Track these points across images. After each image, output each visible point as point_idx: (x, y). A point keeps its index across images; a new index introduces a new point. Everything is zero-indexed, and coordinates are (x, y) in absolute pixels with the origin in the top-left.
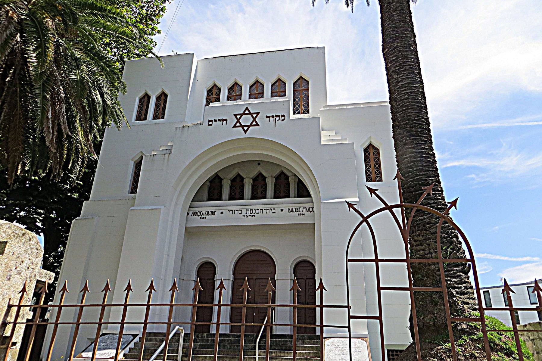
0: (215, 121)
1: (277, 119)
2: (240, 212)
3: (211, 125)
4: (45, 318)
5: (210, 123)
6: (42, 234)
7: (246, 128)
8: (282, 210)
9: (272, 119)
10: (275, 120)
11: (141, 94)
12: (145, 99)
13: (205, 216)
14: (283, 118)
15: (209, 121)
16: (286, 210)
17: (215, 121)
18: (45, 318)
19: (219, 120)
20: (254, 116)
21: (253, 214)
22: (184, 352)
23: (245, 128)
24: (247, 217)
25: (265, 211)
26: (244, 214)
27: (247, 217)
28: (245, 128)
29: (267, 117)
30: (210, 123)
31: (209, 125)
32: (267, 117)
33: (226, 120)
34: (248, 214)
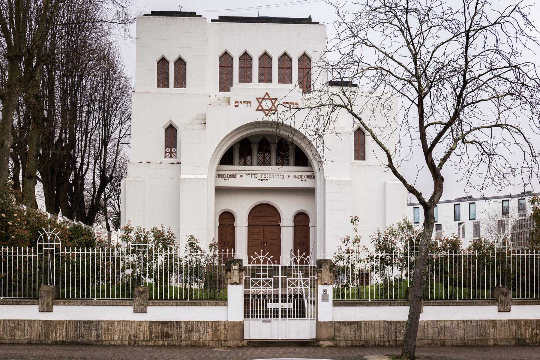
0: (241, 102)
2: (256, 176)
3: (237, 106)
5: (237, 104)
8: (289, 176)
13: (228, 178)
15: (236, 102)
16: (292, 176)
17: (241, 102)
19: (244, 102)
21: (266, 179)
30: (237, 104)
31: (236, 106)
33: (250, 103)
34: (262, 178)
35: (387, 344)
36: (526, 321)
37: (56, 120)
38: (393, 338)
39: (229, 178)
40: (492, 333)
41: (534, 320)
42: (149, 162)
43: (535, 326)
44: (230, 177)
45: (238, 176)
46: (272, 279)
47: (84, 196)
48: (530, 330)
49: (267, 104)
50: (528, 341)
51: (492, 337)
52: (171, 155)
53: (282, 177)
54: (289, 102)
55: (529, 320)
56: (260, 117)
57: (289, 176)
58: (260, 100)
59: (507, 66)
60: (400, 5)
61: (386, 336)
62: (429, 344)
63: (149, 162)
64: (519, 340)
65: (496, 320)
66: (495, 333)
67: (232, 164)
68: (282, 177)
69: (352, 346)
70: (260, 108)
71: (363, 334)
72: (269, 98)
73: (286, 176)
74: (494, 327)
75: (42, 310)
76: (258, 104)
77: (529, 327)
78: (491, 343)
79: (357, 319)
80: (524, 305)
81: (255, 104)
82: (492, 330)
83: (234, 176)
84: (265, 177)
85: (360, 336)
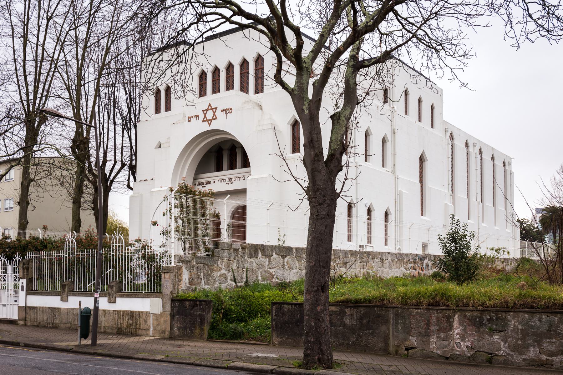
1: (228, 112)
2: (224, 180)
5: (189, 119)
7: (210, 122)
10: (226, 113)
14: (231, 111)
15: (189, 118)
23: (209, 122)
25: (239, 179)
26: (227, 182)
28: (209, 122)
29: (222, 111)
30: (189, 119)
34: (229, 182)
35: (49, 326)
36: (124, 312)
38: (52, 321)
39: (206, 185)
40: (103, 321)
41: (129, 311)
42: (146, 180)
43: (129, 317)
44: (207, 184)
45: (212, 182)
46: (7, 275)
48: (126, 320)
50: (124, 330)
51: (103, 325)
52: (394, 129)
55: (126, 311)
56: (205, 127)
58: (205, 112)
59: (4, 155)
60: (63, 101)
61: (49, 319)
62: (69, 328)
63: (146, 180)
64: (119, 329)
65: (106, 310)
66: (105, 321)
67: (222, 170)
69: (33, 326)
70: (205, 119)
71: (38, 317)
74: (105, 316)
77: (126, 317)
78: (102, 330)
79: (35, 306)
80: (123, 297)
81: (202, 116)
82: (103, 318)
83: (209, 183)
84: (231, 181)
85: (37, 319)
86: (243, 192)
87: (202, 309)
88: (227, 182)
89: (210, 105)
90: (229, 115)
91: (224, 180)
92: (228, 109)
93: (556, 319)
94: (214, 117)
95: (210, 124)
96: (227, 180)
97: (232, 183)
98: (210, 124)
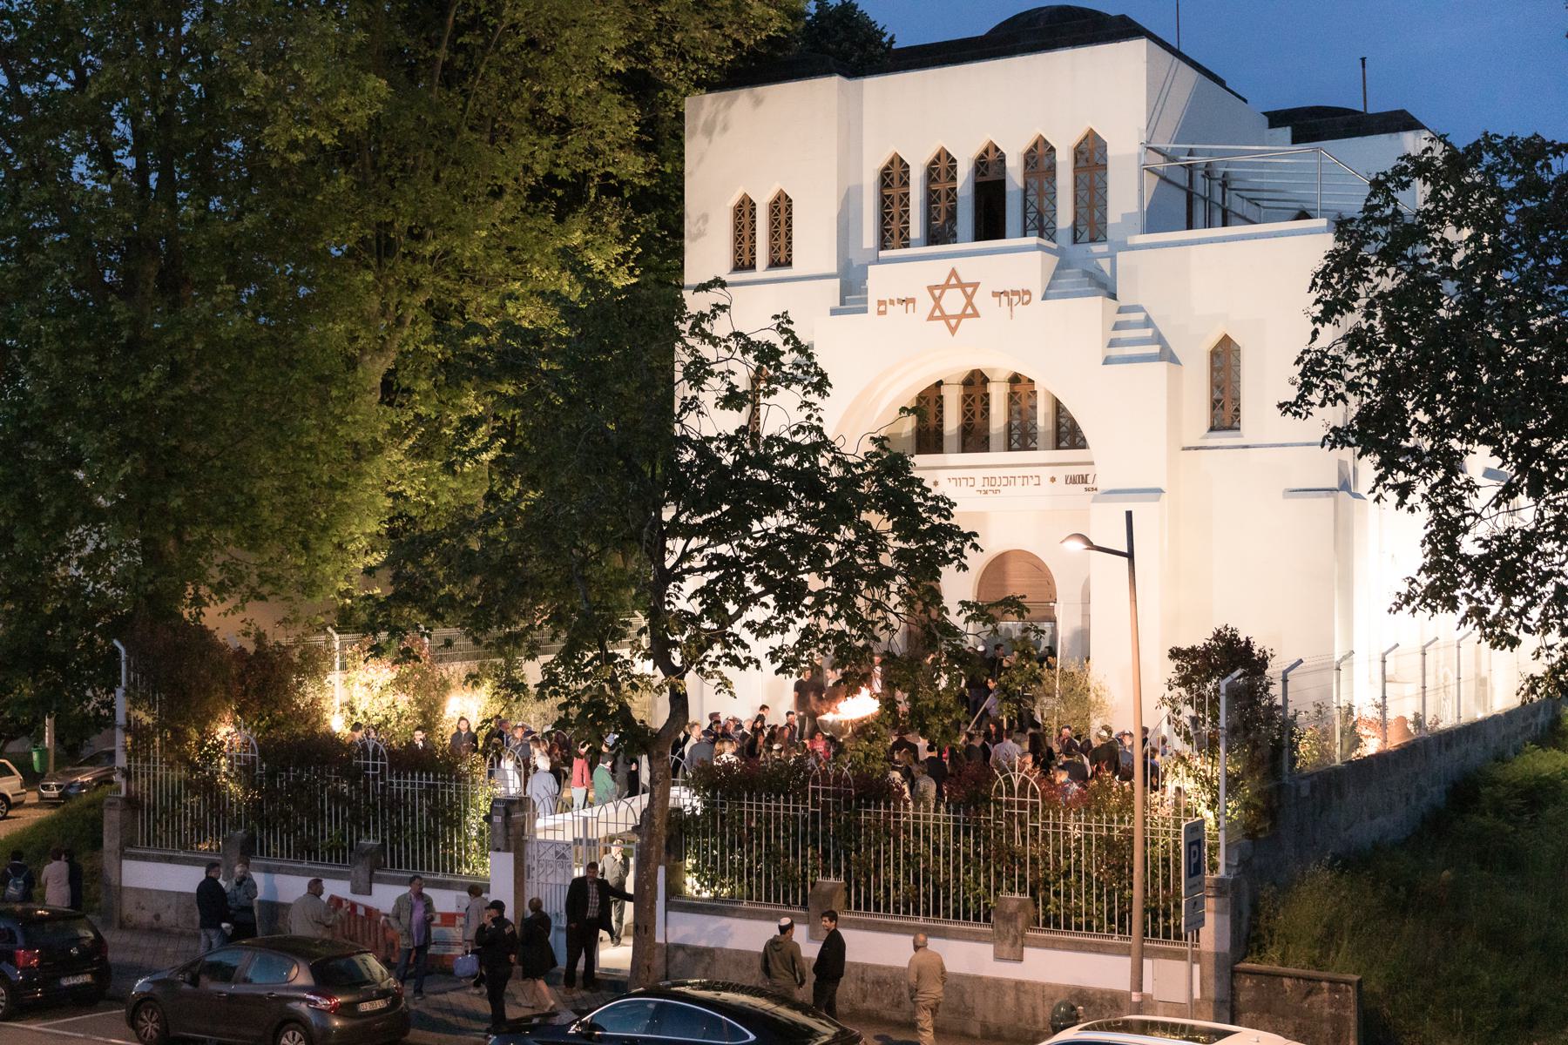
0: (892, 302)
1: (1016, 299)
2: (971, 482)
3: (884, 313)
4: (1289, 129)
5: (882, 308)
6: (636, 612)
7: (953, 322)
9: (1004, 299)
10: (1010, 303)
11: (734, 200)
12: (744, 212)
14: (1026, 298)
15: (881, 303)
16: (1061, 479)
17: (892, 302)
18: (1289, 129)
20: (953, 281)
22: (1100, 907)
23: (954, 281)
24: (986, 492)
25: (1019, 481)
26: (979, 485)
27: (986, 492)
28: (954, 281)
29: (995, 294)
30: (882, 308)
31: (880, 313)
32: (995, 294)
33: (913, 300)
34: (986, 488)
37: (779, 529)
42: (1363, 60)
47: (842, 975)
49: (953, 301)
53: (1036, 480)
54: (1008, 290)
57: (1053, 480)
58: (937, 291)
63: (1363, 60)
67: (987, 450)
68: (1036, 480)
70: (969, 290)
72: (937, 305)
73: (1045, 480)
75: (998, 957)
76: (964, 280)
81: (925, 303)
86: (1112, 344)
87: (1338, 1001)
88: (979, 485)
89: (953, 330)
90: (1019, 309)
91: (971, 482)
92: (1015, 293)
93: (1373, 983)
94: (969, 311)
95: (953, 273)
96: (979, 482)
97: (995, 492)
98: (953, 273)
